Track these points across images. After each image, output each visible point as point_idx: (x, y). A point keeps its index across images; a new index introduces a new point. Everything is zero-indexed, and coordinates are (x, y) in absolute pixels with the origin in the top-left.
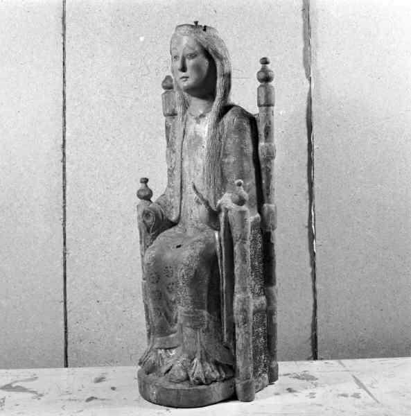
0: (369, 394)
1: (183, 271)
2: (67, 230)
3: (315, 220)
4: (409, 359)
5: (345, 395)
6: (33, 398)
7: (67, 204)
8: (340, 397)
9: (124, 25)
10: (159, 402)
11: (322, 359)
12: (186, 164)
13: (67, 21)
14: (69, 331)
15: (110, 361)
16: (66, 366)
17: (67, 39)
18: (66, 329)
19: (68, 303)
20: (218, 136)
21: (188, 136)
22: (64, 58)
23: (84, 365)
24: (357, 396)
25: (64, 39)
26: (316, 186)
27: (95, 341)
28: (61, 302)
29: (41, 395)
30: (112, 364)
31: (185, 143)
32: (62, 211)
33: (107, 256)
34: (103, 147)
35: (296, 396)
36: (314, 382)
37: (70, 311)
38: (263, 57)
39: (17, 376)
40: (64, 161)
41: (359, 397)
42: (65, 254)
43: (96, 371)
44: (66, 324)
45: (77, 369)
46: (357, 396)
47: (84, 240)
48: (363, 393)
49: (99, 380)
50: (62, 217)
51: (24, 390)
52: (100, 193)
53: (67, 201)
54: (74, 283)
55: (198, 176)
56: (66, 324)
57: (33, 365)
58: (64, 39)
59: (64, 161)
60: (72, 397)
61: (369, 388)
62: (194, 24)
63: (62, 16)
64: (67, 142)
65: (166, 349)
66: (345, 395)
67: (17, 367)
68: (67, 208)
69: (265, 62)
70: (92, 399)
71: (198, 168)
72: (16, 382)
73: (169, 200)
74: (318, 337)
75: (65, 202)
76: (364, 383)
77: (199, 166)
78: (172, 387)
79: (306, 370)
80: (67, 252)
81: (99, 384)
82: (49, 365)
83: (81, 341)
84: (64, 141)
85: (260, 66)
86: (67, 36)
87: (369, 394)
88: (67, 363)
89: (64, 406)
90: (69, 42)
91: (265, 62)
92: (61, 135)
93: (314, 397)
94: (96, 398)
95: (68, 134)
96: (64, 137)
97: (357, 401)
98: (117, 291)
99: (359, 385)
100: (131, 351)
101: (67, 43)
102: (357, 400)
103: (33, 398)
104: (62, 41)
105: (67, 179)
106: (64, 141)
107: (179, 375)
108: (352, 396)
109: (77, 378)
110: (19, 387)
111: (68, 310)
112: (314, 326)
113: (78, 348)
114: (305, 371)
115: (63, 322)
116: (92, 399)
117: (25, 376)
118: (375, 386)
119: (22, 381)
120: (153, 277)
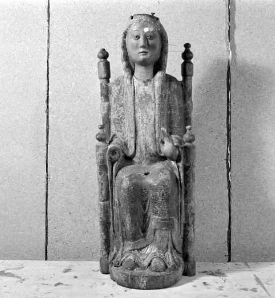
0: (264, 288)
1: (163, 190)
2: (49, 161)
3: (230, 157)
4: (274, 263)
5: (246, 290)
6: (17, 282)
7: (49, 143)
8: (242, 291)
9: (92, 12)
10: (149, 287)
11: (234, 261)
12: (138, 115)
13: (51, 10)
14: (49, 234)
15: (78, 257)
16: (46, 259)
17: (50, 23)
18: (47, 232)
19: (48, 213)
20: (164, 95)
21: (138, 94)
22: (48, 37)
23: (58, 259)
24: (254, 290)
25: (49, 24)
26: (233, 131)
27: (67, 242)
28: (43, 213)
29: (24, 280)
30: (79, 259)
31: (137, 101)
32: (45, 148)
33: (78, 181)
34: (75, 101)
35: (208, 288)
36: (224, 278)
37: (50, 220)
38: (103, 48)
39: (10, 265)
40: (47, 111)
41: (256, 291)
42: (47, 179)
43: (65, 264)
44: (47, 229)
45: (52, 262)
46: (254, 290)
47: (61, 168)
48: (259, 288)
49: (66, 271)
50: (45, 152)
51: (12, 275)
52: (73, 135)
53: (49, 140)
54: (53, 200)
55: (150, 123)
56: (47, 229)
57: (23, 258)
58: (49, 24)
59: (47, 111)
60: (45, 282)
61: (265, 285)
62: (151, 15)
63: (47, 7)
64: (50, 98)
65: (138, 250)
66: (246, 290)
67: (12, 259)
68: (49, 145)
69: (187, 46)
70: (59, 284)
71: (149, 117)
72: (8, 269)
73: (123, 141)
74: (232, 244)
75: (48, 141)
76: (262, 281)
77: (151, 116)
78: (158, 274)
79: (219, 269)
80: (48, 178)
81: (67, 274)
82: (34, 257)
83: (57, 242)
84: (48, 97)
85: (183, 49)
86: (50, 21)
87: (264, 288)
88: (47, 257)
89: (38, 288)
90: (52, 25)
91: (187, 46)
92: (46, 93)
93: (222, 290)
94: (62, 284)
95: (50, 93)
96: (48, 94)
97: (254, 294)
98: (84, 206)
99: (258, 282)
100: (92, 251)
101: (50, 27)
102: (254, 293)
103: (17, 282)
104: (47, 25)
105: (50, 125)
106: (48, 97)
107: (161, 266)
108: (251, 290)
109: (52, 269)
110: (10, 273)
111: (48, 219)
112: (229, 239)
113: (55, 247)
114: (219, 270)
115: (44, 228)
116: (59, 284)
117: (14, 263)
118: (269, 283)
119: (11, 269)
120: (133, 198)
